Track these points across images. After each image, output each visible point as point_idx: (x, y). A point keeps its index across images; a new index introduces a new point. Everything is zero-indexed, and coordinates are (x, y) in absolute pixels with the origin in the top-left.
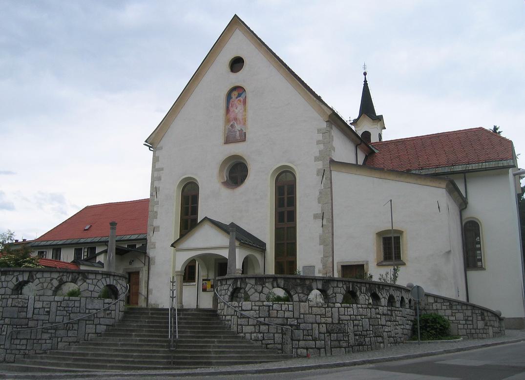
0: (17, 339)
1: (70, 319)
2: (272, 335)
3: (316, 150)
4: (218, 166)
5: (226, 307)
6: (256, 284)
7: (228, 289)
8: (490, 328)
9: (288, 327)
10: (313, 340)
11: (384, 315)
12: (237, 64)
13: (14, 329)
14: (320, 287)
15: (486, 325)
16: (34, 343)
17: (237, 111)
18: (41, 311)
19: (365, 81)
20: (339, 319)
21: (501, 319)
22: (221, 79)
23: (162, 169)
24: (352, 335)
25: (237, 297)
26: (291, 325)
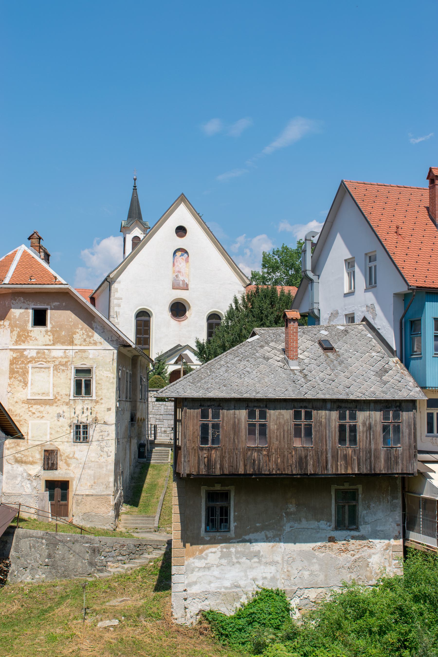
17: (180, 266)
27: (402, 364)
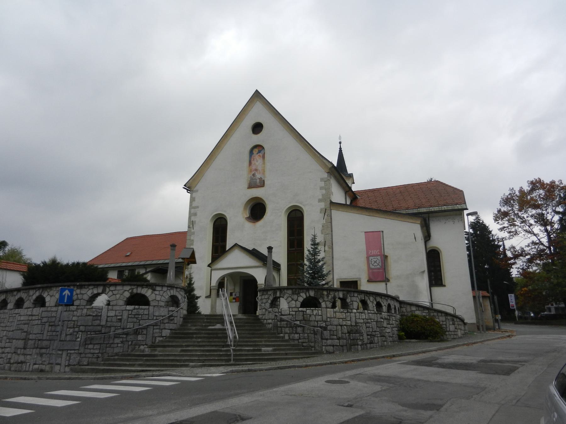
0: (91, 344)
1: (140, 325)
2: (306, 335)
3: (319, 194)
4: (244, 205)
5: (267, 313)
6: (293, 294)
7: (268, 298)
8: (459, 330)
9: (318, 328)
10: (337, 339)
11: (385, 319)
12: (257, 128)
13: (89, 336)
14: (341, 296)
15: (456, 328)
16: (106, 347)
17: (257, 164)
18: (114, 319)
19: (340, 148)
20: (356, 323)
21: (465, 324)
22: (245, 139)
23: (198, 207)
24: (365, 335)
25: (275, 304)
26: (321, 327)
27: (520, 370)
